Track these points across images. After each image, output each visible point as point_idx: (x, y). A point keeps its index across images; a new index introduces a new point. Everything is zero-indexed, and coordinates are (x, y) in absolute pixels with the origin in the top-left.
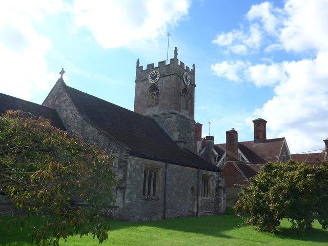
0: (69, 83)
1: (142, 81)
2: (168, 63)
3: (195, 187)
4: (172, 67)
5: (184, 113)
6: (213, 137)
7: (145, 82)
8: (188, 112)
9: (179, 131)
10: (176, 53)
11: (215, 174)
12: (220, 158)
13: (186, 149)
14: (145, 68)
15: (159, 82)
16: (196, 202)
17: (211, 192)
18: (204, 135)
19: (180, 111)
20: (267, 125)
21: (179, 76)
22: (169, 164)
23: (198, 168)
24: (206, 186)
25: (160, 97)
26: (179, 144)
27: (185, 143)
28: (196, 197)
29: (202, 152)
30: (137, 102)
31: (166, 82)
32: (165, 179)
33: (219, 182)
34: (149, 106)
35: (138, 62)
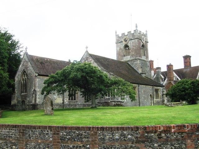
0: (91, 52)
1: (120, 42)
2: (132, 32)
3: (152, 95)
4: (135, 34)
5: (143, 58)
6: (160, 68)
7: (121, 43)
8: (145, 57)
9: (142, 68)
10: (137, 27)
11: (161, 88)
12: (165, 79)
13: (146, 77)
14: (120, 35)
15: (129, 43)
16: (153, 101)
17: (52, 118)
18: (155, 66)
19: (141, 57)
20: (191, 58)
21: (139, 39)
22: (140, 85)
23: (153, 86)
24: (157, 94)
25: (130, 51)
26: (142, 75)
27: (145, 74)
28: (153, 99)
29: (155, 77)
30: (118, 54)
31: (133, 42)
32: (139, 91)
33: (163, 92)
34: (124, 56)
35: (116, 32)
